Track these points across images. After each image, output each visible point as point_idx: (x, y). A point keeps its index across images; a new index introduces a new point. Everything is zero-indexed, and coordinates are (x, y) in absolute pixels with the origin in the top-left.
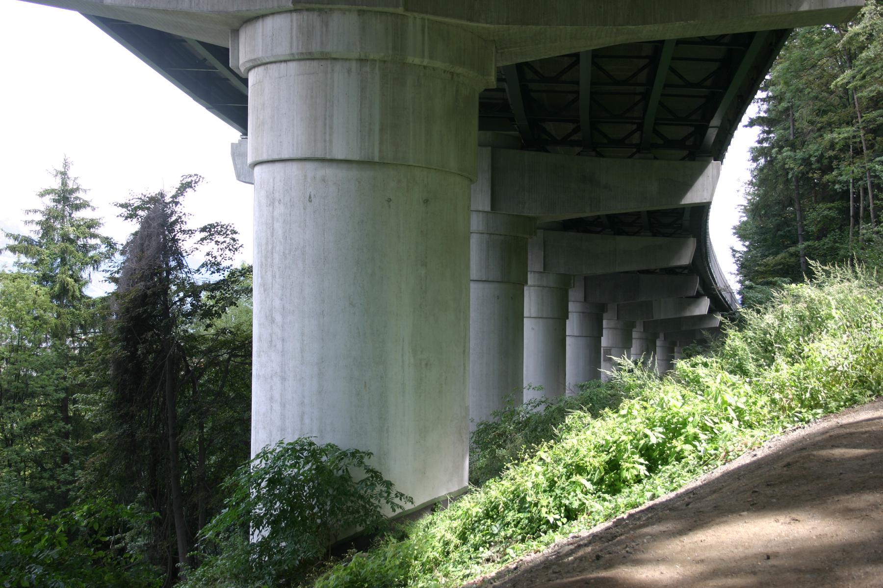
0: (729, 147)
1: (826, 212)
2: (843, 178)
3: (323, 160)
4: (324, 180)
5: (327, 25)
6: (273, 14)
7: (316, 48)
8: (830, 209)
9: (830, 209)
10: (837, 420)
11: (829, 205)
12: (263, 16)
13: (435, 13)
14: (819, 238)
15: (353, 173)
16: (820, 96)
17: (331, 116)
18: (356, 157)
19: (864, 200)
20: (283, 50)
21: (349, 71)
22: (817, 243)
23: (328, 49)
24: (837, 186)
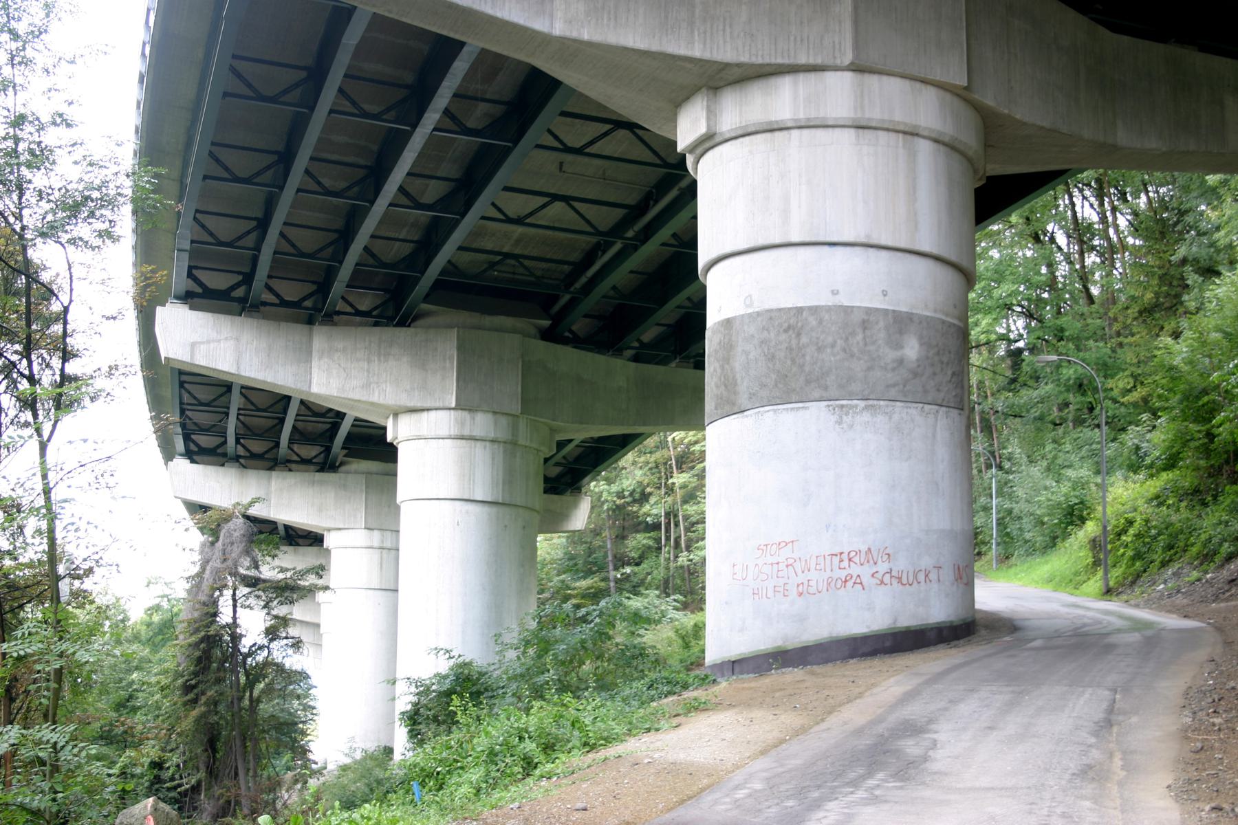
0: (156, 443)
1: (645, 542)
2: (655, 511)
3: (509, 505)
4: (467, 512)
5: (474, 419)
6: (436, 409)
7: (466, 433)
8: (649, 538)
9: (649, 538)
10: (1017, 401)
11: (648, 535)
12: (428, 410)
13: (535, 416)
14: (637, 564)
15: (494, 509)
16: (1111, 583)
17: (474, 474)
18: (489, 500)
19: (675, 532)
20: (444, 432)
21: (485, 447)
22: (636, 569)
23: (474, 434)
24: (648, 519)
